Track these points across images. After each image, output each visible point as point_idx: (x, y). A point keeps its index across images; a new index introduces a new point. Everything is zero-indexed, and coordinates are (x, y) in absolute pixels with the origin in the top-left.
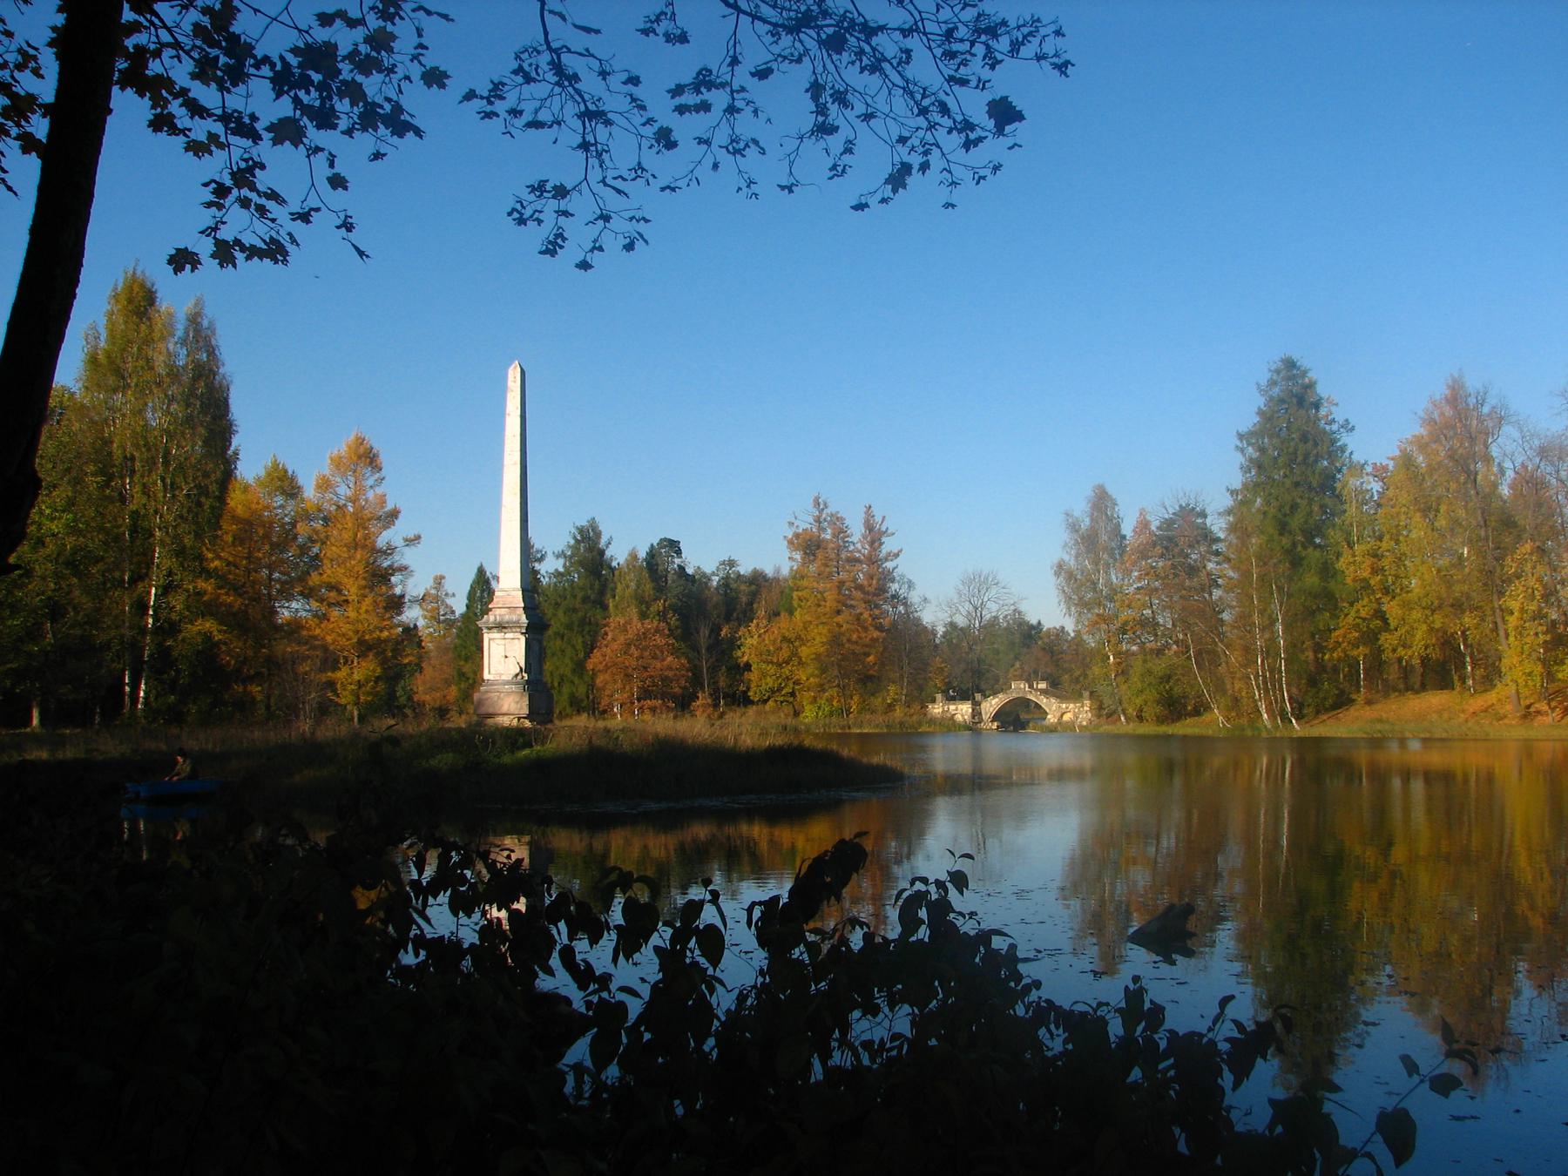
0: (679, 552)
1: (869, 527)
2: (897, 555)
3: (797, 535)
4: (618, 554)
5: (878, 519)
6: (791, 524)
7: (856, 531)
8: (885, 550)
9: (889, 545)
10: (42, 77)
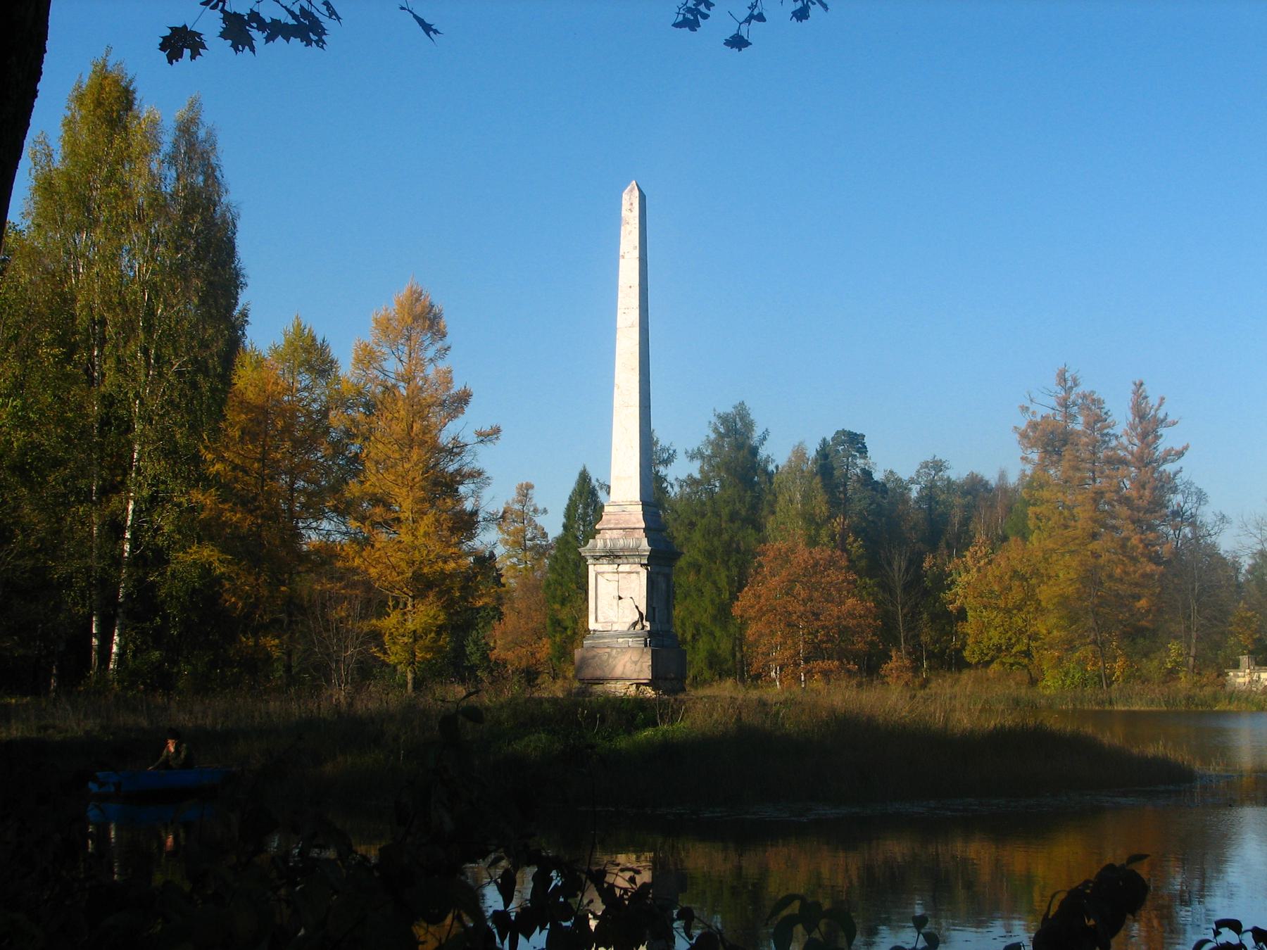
0: (863, 451)
1: (1140, 413)
2: (1180, 454)
3: (1034, 426)
4: (777, 452)
5: (1153, 400)
6: (1025, 409)
7: (1121, 418)
8: (1162, 446)
9: (1168, 440)
10: (1186, 448)
